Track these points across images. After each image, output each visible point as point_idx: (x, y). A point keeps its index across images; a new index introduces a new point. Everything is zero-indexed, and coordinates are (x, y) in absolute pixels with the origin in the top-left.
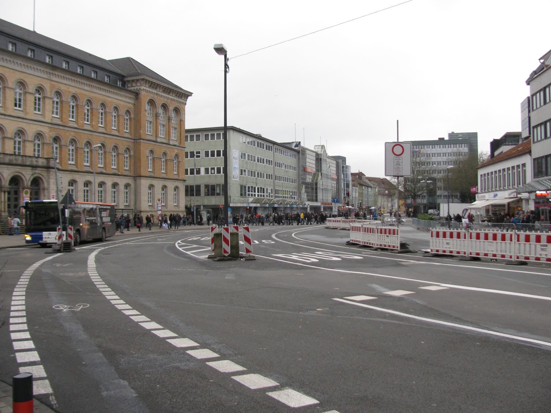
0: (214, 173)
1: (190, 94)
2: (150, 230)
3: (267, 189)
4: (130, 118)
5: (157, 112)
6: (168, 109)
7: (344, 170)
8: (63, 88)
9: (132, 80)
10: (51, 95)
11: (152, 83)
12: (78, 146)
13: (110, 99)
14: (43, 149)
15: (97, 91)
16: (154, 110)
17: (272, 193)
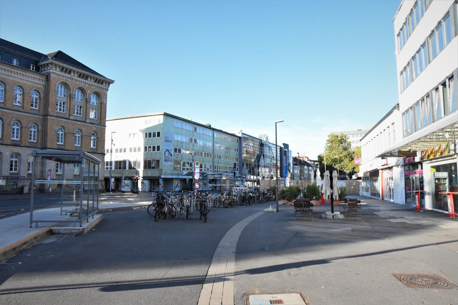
0: (151, 151)
1: (112, 82)
3: (205, 165)
5: (71, 93)
6: (86, 92)
7: (286, 153)
11: (63, 68)
12: (66, 132)
16: (68, 92)
17: (211, 168)
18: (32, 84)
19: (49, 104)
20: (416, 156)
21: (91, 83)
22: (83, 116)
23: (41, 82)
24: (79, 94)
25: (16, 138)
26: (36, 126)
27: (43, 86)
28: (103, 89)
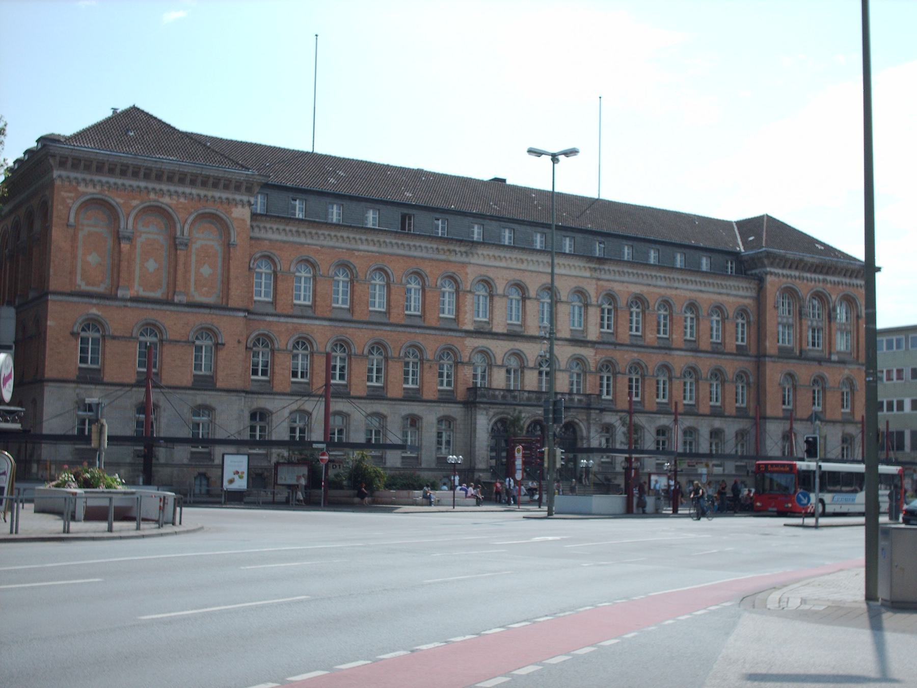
2: (540, 507)
4: (749, 323)
8: (617, 287)
9: (213, 176)
10: (597, 301)
13: (705, 296)
14: (585, 380)
15: (680, 285)
19: (766, 333)
22: (825, 347)
23: (749, 294)
24: (784, 301)
25: (447, 385)
26: (417, 352)
27: (753, 300)
28: (859, 288)
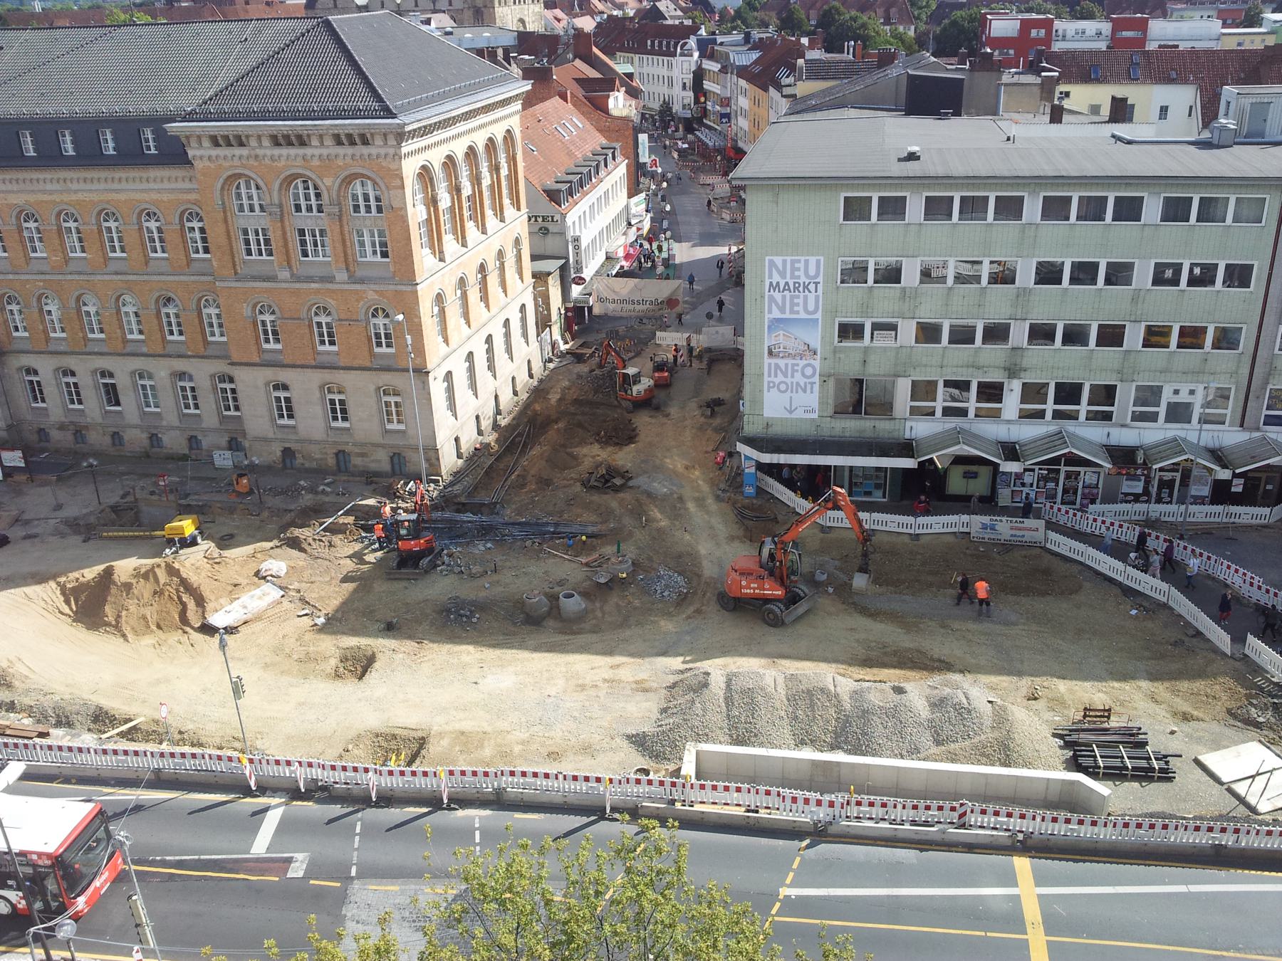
18: (172, 197)
20: (1126, 99)
21: (325, 152)
